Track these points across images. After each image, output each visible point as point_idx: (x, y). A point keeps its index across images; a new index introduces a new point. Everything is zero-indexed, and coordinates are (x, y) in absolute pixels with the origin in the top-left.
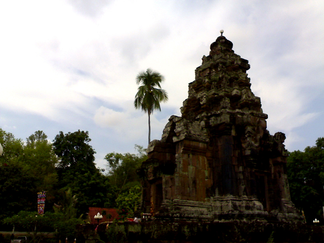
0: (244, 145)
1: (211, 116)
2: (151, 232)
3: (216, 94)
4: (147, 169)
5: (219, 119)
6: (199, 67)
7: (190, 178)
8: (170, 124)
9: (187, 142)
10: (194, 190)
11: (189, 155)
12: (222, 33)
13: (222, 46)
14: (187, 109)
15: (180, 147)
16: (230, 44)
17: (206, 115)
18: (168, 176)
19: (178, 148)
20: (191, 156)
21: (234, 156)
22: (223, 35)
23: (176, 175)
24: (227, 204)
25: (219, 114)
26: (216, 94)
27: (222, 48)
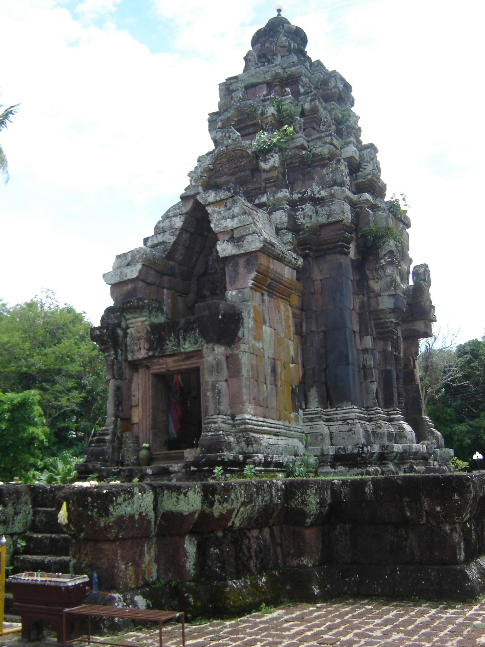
0: (375, 286)
1: (302, 201)
2: (233, 510)
3: (304, 149)
4: (125, 330)
5: (323, 211)
6: (236, 78)
7: (266, 357)
8: (184, 210)
9: (263, 260)
10: (274, 391)
11: (263, 295)
12: (279, 11)
13: (278, 41)
14: (209, 178)
15: (241, 270)
16: (299, 37)
17: (288, 194)
18: (220, 350)
19: (236, 273)
20: (266, 298)
21: (353, 309)
22: (283, 14)
23: (243, 347)
24: (347, 428)
25: (322, 199)
26: (304, 149)
27: (290, 45)
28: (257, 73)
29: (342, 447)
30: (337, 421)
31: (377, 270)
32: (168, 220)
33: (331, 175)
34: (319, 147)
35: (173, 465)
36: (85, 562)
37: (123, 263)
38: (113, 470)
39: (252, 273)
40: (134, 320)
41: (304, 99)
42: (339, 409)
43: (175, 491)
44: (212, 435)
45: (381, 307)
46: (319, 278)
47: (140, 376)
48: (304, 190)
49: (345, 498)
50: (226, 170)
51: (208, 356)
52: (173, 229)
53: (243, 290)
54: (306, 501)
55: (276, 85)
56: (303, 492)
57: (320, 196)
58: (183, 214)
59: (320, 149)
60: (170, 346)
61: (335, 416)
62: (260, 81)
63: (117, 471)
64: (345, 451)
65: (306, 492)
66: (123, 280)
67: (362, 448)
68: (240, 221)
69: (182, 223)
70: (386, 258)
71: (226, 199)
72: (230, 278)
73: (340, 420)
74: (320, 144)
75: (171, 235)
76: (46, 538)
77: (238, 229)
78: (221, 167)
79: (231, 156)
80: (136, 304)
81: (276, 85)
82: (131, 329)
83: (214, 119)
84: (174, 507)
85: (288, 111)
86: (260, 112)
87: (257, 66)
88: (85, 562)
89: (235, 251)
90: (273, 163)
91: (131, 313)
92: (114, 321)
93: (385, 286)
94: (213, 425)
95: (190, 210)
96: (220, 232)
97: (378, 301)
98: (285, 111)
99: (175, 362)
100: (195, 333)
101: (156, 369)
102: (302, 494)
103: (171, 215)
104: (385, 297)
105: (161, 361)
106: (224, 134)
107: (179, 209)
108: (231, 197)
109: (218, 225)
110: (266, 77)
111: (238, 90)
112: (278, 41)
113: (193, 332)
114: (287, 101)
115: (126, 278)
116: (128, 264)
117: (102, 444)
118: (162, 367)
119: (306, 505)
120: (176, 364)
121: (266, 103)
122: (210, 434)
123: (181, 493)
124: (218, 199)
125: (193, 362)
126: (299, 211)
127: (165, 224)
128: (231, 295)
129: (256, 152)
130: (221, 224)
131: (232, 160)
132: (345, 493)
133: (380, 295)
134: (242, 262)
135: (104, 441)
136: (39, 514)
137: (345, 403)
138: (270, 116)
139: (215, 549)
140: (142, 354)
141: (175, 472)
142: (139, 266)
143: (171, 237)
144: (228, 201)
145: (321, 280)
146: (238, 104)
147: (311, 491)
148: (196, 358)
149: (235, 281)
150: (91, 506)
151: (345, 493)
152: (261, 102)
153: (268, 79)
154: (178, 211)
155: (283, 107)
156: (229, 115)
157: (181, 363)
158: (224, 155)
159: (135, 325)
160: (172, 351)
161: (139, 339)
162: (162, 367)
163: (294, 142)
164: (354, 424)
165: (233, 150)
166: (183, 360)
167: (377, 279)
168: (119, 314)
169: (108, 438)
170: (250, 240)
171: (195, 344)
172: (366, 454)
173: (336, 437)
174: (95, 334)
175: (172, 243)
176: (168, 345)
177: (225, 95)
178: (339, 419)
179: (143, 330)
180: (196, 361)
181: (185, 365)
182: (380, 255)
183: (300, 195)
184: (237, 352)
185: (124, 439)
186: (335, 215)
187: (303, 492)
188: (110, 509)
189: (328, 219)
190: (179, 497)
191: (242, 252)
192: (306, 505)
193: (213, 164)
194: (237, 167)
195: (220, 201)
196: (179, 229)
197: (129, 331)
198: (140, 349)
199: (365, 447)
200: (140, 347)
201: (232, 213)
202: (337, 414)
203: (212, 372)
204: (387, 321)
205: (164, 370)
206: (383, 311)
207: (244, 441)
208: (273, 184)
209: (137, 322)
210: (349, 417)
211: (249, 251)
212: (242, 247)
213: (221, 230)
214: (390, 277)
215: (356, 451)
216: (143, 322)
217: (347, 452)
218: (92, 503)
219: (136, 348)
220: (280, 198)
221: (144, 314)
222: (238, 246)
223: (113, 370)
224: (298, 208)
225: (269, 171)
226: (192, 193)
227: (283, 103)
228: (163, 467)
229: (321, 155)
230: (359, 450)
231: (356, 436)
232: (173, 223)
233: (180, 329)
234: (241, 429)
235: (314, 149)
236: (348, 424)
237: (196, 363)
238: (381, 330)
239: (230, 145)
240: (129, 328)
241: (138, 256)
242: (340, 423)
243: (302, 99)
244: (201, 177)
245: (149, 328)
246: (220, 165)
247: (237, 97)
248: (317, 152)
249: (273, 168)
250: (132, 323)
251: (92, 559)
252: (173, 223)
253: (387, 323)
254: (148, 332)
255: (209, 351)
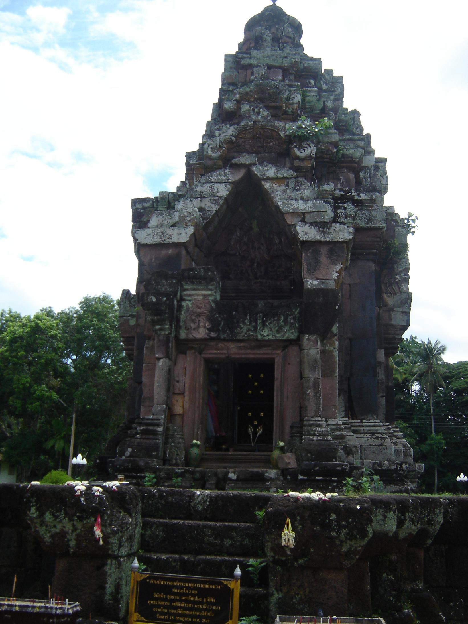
15: (323, 259)
22: (278, 4)
24: (377, 442)
28: (274, 55)
29: (378, 462)
30: (364, 433)
31: (391, 284)
32: (209, 185)
33: (369, 180)
34: (351, 148)
35: (269, 471)
36: (298, 597)
37: (165, 222)
38: (177, 471)
39: (337, 264)
40: (194, 292)
41: (327, 96)
42: (364, 421)
43: (381, 507)
44: (318, 440)
45: (393, 322)
46: (348, 282)
47: (188, 359)
48: (347, 189)
49: (451, 518)
50: (248, 147)
51: (310, 349)
52: (214, 196)
53: (328, 281)
54: (433, 520)
55: (291, 74)
56: (430, 510)
57: (360, 198)
58: (229, 183)
59: (351, 151)
60: (244, 329)
61: (362, 428)
62: (277, 64)
63: (182, 472)
64: (381, 466)
65: (434, 511)
66: (165, 242)
67: (401, 465)
68: (314, 205)
69: (228, 193)
70: (402, 274)
71: (288, 178)
72: (309, 265)
73: (367, 433)
74: (352, 145)
75: (213, 203)
76: (175, 560)
77: (312, 214)
78: (244, 142)
79: (258, 133)
80: (202, 273)
81: (291, 74)
82: (187, 302)
83: (231, 89)
84: (379, 526)
85: (312, 104)
86: (285, 96)
87: (273, 48)
88: (298, 597)
89: (318, 237)
90: (309, 153)
91: (193, 283)
92: (166, 289)
93: (399, 302)
94: (318, 429)
95: (239, 180)
96: (289, 213)
97: (390, 316)
98: (309, 103)
99: (240, 348)
100: (279, 319)
101: (212, 353)
102: (429, 513)
103: (213, 180)
104: (399, 313)
105: (220, 345)
106: (252, 108)
107: (225, 176)
108: (295, 178)
109: (287, 204)
110: (284, 62)
111: (260, 66)
112: (273, 30)
113: (276, 318)
114: (313, 94)
115: (168, 241)
116: (173, 225)
117: (151, 436)
118: (221, 352)
119: (432, 525)
120: (240, 352)
121: (292, 89)
122: (315, 438)
123: (390, 510)
124: (280, 176)
125: (266, 352)
126: (341, 209)
127: (204, 189)
128: (312, 284)
129: (290, 136)
130: (291, 204)
131: (258, 137)
132: (452, 513)
133: (393, 310)
134: (324, 250)
135: (155, 433)
136: (151, 527)
137: (370, 415)
138: (296, 104)
139: (389, 575)
140: (201, 333)
141: (271, 479)
142: (191, 230)
143: (213, 206)
144: (290, 181)
145: (350, 285)
146: (261, 82)
147: (440, 511)
148: (271, 348)
149: (315, 270)
150: (335, 525)
151: (452, 513)
152: (287, 87)
153: (286, 65)
154: (224, 178)
155: (308, 99)
156: (248, 90)
157: (249, 351)
158: (250, 131)
159: (193, 298)
160: (248, 336)
161: (199, 315)
162: (221, 352)
163: (328, 137)
164: (385, 439)
165: (263, 128)
166: (252, 348)
167: (390, 293)
168: (174, 281)
169: (161, 429)
170: (337, 229)
171: (278, 332)
172: (404, 471)
173: (365, 450)
174: (149, 300)
175: (214, 212)
176: (241, 328)
177: (231, 68)
178: (366, 431)
179: (205, 306)
180: (270, 351)
181: (253, 354)
182: (396, 270)
183: (342, 193)
184: (332, 349)
185: (171, 433)
186: (375, 222)
187: (430, 510)
188: (368, 530)
189: (368, 223)
190: (388, 515)
191: (328, 239)
192: (432, 525)
193: (236, 136)
194: (262, 147)
195: (281, 178)
196: (223, 198)
197: (184, 304)
198: (198, 327)
199: (404, 464)
200: (199, 325)
201: (300, 195)
202: (362, 426)
203: (315, 367)
204: (396, 337)
205: (223, 356)
206: (394, 326)
207: (342, 449)
208: (303, 174)
209: (198, 295)
210: (377, 430)
211: (335, 240)
212: (328, 234)
213: (291, 211)
214: (405, 294)
215: (393, 467)
216: (205, 296)
217: (383, 468)
218: (338, 521)
219: (193, 325)
220: (327, 191)
221: (210, 287)
222: (323, 232)
223: (168, 347)
224: (340, 206)
225: (302, 160)
226: (247, 163)
227: (308, 94)
228: (257, 472)
229: (352, 157)
230: (397, 467)
231: (388, 451)
232: (216, 190)
233: (259, 313)
234: (336, 435)
235: (345, 150)
236: (377, 438)
237: (269, 354)
238: (387, 346)
239: (259, 121)
240: (185, 300)
241: (188, 219)
242: (368, 436)
243: (325, 95)
244: (220, 146)
245: (213, 305)
246: (243, 140)
247: (259, 74)
248: (348, 152)
249: (309, 157)
250: (190, 295)
251: (310, 592)
252: (216, 190)
253: (395, 338)
254: (212, 310)
255: (311, 343)
